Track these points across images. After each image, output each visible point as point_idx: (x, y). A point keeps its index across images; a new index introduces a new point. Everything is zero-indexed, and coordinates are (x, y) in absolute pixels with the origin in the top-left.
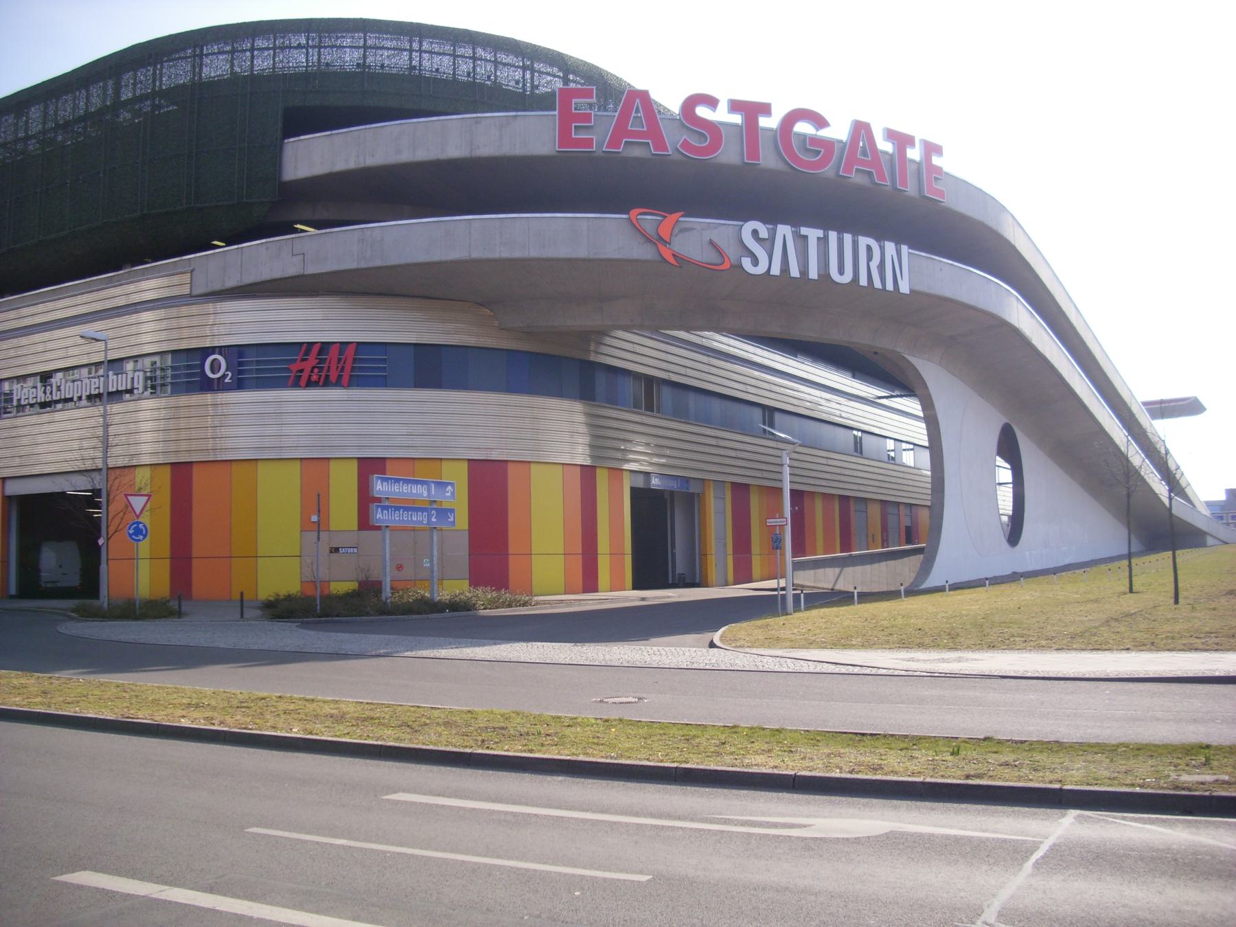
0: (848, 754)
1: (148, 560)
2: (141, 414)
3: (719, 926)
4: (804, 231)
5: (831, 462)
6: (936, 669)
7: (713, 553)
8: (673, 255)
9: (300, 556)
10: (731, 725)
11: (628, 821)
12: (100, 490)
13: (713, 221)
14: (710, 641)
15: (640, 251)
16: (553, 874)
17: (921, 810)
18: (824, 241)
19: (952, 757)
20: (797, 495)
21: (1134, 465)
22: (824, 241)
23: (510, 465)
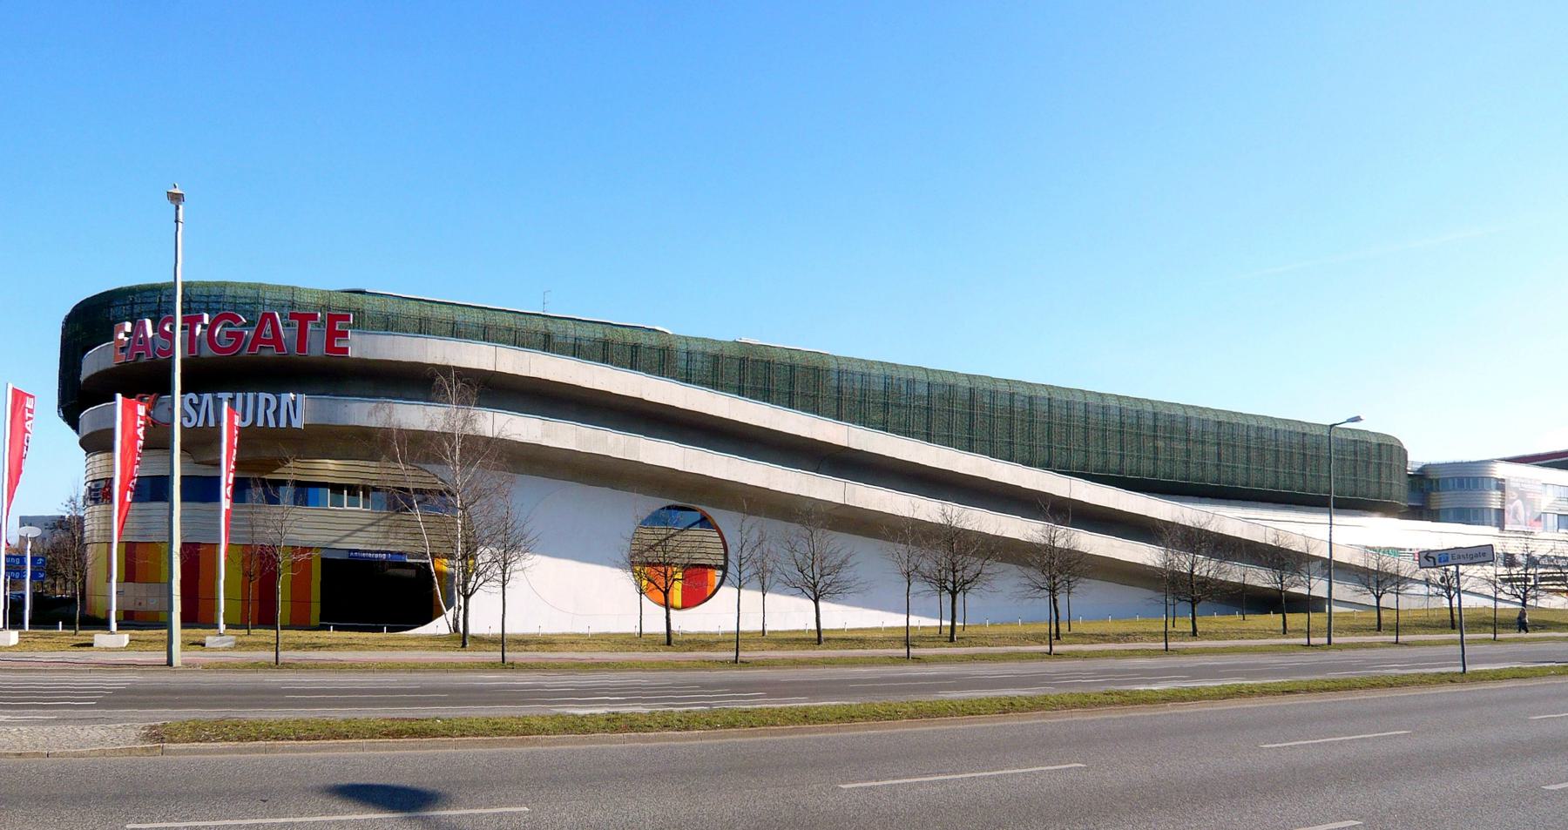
1: (736, 629)
4: (220, 395)
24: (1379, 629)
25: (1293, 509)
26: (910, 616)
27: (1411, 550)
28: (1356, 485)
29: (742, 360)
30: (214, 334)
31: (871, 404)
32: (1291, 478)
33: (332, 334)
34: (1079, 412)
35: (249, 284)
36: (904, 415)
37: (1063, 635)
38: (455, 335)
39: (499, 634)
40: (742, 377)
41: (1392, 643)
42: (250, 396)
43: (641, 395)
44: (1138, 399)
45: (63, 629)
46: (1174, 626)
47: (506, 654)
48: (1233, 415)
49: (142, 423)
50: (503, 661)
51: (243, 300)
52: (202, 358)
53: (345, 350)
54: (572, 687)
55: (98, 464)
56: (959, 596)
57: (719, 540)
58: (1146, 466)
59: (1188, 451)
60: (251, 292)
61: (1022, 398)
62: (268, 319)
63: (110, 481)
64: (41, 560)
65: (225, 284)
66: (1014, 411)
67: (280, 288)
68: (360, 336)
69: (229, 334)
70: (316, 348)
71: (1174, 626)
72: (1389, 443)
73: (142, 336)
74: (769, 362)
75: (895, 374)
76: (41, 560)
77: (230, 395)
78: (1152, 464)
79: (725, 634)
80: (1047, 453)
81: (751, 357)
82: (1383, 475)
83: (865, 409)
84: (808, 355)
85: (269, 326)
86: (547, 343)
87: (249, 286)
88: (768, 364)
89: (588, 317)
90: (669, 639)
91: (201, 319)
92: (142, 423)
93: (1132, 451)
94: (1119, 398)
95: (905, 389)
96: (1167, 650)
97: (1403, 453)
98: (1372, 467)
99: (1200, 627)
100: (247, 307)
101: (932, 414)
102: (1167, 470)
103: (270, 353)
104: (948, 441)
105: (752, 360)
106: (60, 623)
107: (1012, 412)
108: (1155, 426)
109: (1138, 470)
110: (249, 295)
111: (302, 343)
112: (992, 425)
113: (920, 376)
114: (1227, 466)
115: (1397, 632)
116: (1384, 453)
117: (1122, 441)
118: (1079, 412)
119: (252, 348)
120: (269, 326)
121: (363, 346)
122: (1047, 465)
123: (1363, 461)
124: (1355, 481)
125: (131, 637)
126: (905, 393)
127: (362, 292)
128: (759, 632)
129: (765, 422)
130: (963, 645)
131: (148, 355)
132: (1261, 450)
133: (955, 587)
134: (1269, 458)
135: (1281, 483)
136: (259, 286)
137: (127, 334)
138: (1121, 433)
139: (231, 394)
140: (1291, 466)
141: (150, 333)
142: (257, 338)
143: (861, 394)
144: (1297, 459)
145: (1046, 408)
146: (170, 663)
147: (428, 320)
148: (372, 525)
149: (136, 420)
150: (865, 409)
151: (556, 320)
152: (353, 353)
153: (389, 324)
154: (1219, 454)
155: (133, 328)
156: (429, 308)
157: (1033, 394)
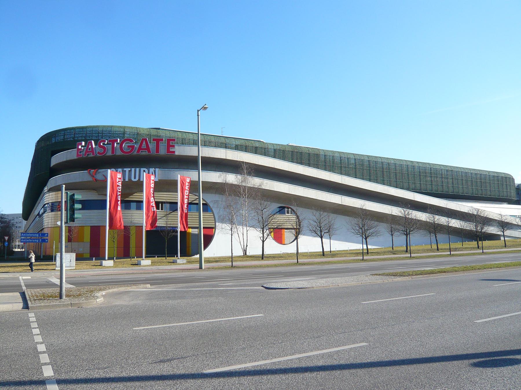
0: (480, 330)
1: (330, 250)
2: (54, 219)
3: (212, 389)
4: (125, 169)
5: (38, 227)
6: (489, 271)
7: (187, 184)
8: (95, 179)
9: (232, 266)
10: (46, 195)
11: (486, 320)
12: (99, 257)
13: (104, 170)
14: (205, 251)
15: (90, 179)
16: (510, 354)
17: (340, 364)
18: (130, 171)
19: (53, 213)
20: (18, 245)
21: (515, 183)
22: (130, 171)
23: (101, 226)
24: (263, 259)
25: (478, 202)
26: (363, 245)
27: (519, 216)
28: (499, 193)
29: (292, 152)
30: (123, 146)
31: (336, 167)
32: (478, 191)
33: (169, 146)
34: (379, 165)
35: (121, 126)
36: (347, 171)
37: (265, 257)
38: (194, 144)
39: (231, 256)
40: (293, 158)
41: (361, 260)
42: (138, 169)
43: (274, 167)
44: (424, 163)
45: (95, 260)
46: (462, 246)
47: (299, 260)
48: (456, 168)
49: (188, 184)
50: (298, 263)
51: (119, 132)
52: (117, 155)
53: (174, 152)
54: (365, 267)
55: (50, 197)
56: (408, 236)
57: (213, 219)
58: (429, 187)
59: (432, 181)
60: (121, 129)
61: (386, 164)
62: (144, 141)
63: (60, 202)
64: (46, 234)
65: (112, 127)
66: (384, 169)
67: (132, 128)
68: (179, 147)
69: (129, 146)
70: (163, 151)
71: (462, 246)
72: (509, 177)
73: (90, 146)
74: (301, 152)
75: (343, 156)
76: (46, 234)
77: (129, 169)
78: (431, 187)
79: (229, 256)
80: (395, 184)
81: (295, 151)
82: (508, 189)
83: (334, 169)
84: (314, 149)
85: (144, 143)
86: (237, 148)
87: (121, 127)
88: (301, 153)
89: (236, 137)
90: (323, 254)
91: (117, 140)
92: (188, 184)
93: (424, 182)
94: (368, 156)
95: (347, 161)
96: (483, 253)
97: (513, 180)
98: (504, 186)
99: (440, 247)
100: (121, 135)
101: (356, 170)
102: (436, 189)
103: (144, 153)
104: (376, 181)
105: (296, 152)
106: (94, 258)
107: (383, 169)
108: (431, 173)
109: (426, 189)
110: (121, 131)
111: (157, 151)
112: (377, 174)
113: (352, 157)
114: (456, 187)
115: (483, 249)
116: (508, 180)
117: (420, 178)
118: (379, 165)
119: (138, 151)
120: (144, 143)
121: (180, 151)
122: (408, 189)
123: (501, 184)
124: (490, 190)
125: (152, 261)
126: (347, 163)
127: (159, 129)
128: (329, 251)
129: (315, 175)
130: (509, 248)
131: (93, 154)
132: (467, 181)
133: (407, 233)
134: (469, 183)
135: (474, 193)
136: (124, 127)
137: (82, 146)
138: (420, 175)
139: (130, 169)
140: (477, 186)
141: (94, 146)
142: (140, 148)
143: (333, 163)
144: (479, 184)
145: (394, 167)
146: (201, 268)
147: (185, 139)
148: (164, 216)
149: (150, 181)
150: (334, 169)
151: (228, 138)
152: (177, 153)
153: (184, 142)
154: (453, 182)
155: (85, 144)
156: (185, 135)
157: (389, 162)
